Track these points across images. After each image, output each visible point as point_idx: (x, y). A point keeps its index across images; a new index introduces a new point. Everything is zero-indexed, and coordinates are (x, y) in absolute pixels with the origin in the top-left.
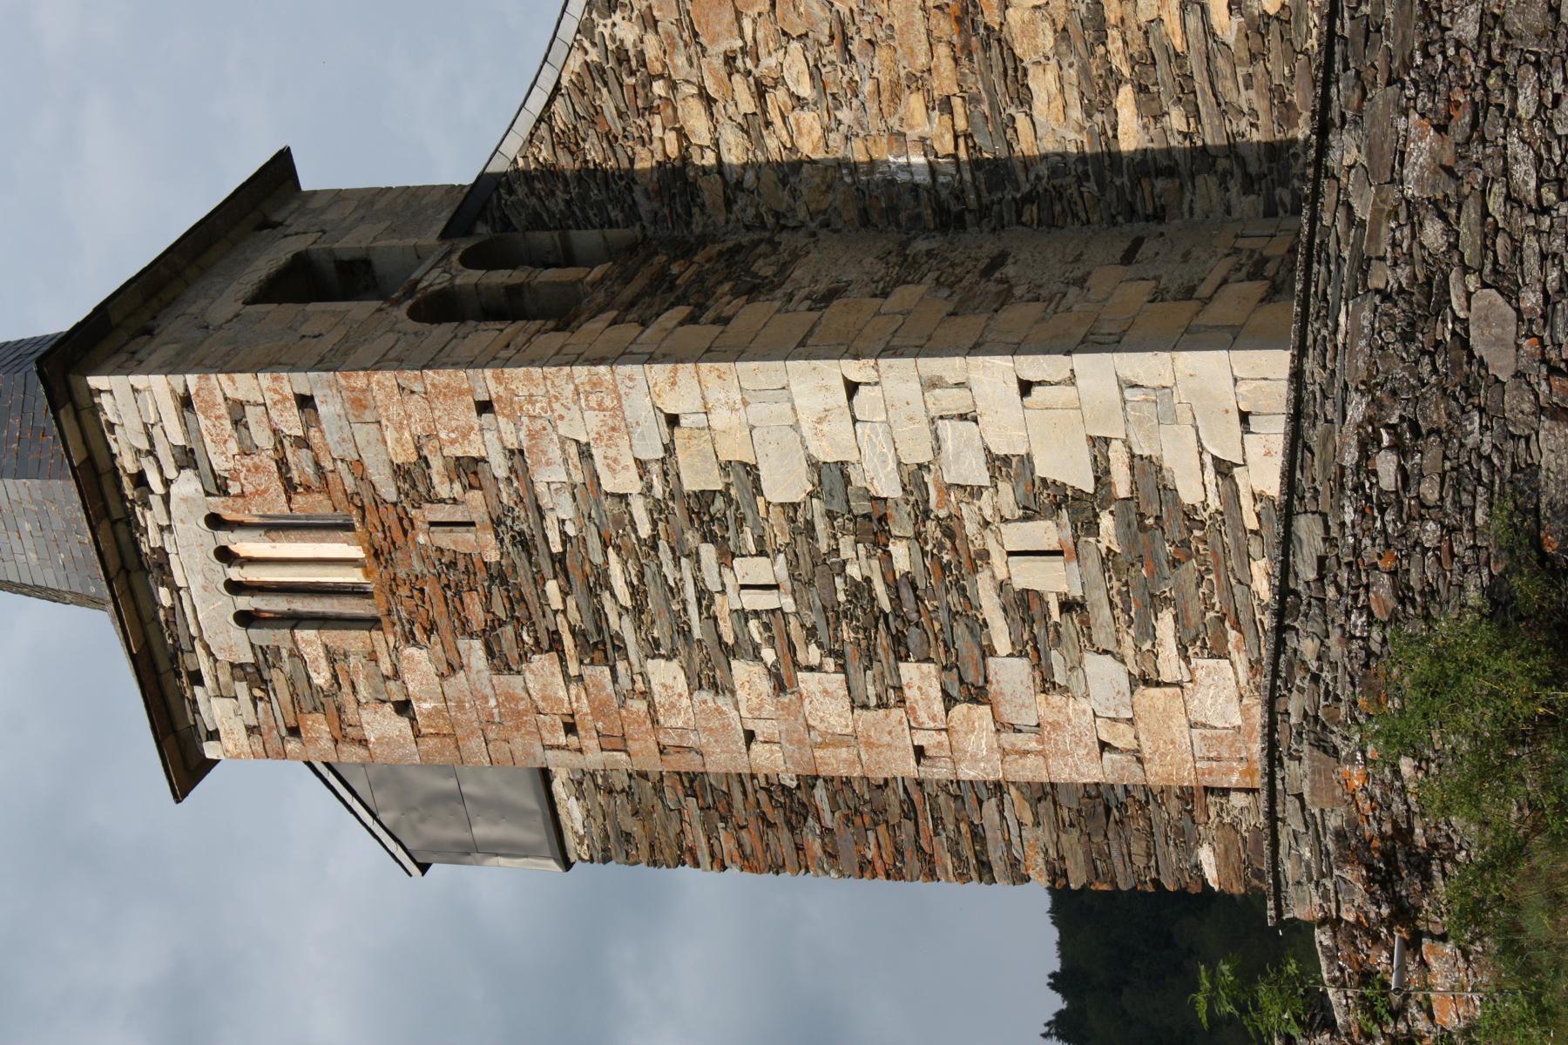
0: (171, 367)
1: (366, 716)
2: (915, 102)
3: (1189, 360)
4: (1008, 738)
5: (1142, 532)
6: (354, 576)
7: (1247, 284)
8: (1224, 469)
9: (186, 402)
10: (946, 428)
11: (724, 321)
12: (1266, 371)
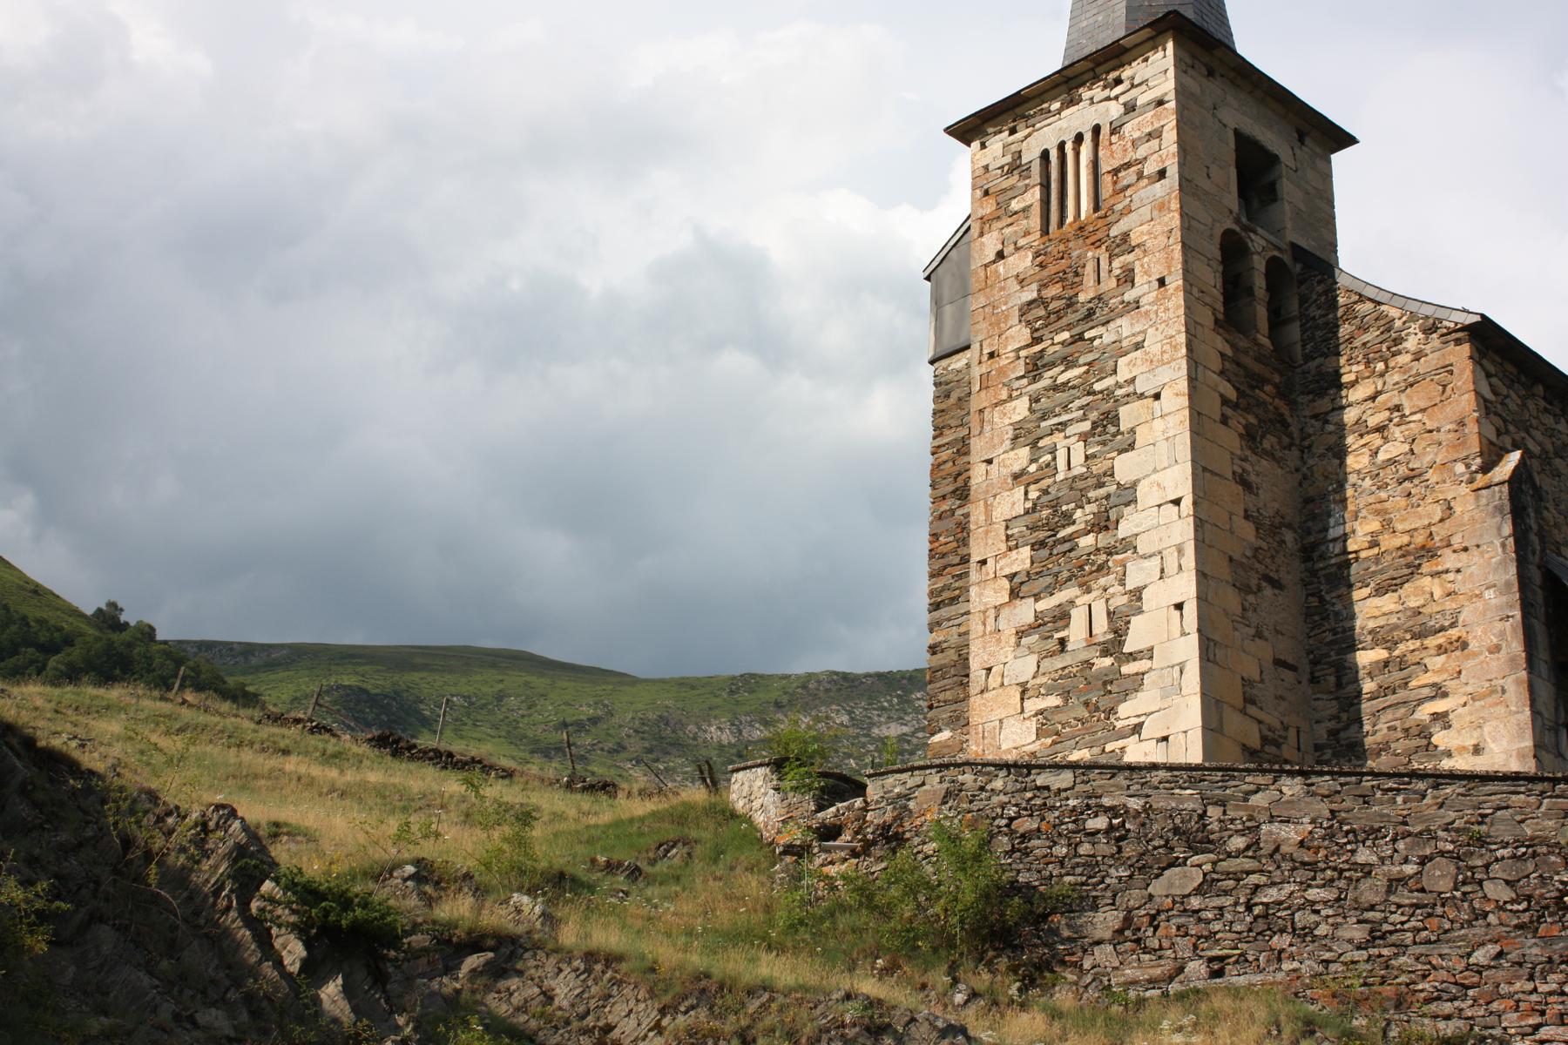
0: (1181, 91)
1: (995, 234)
2: (1375, 525)
3: (1195, 703)
4: (992, 613)
5: (1101, 685)
6: (1070, 219)
7: (1257, 736)
8: (1137, 729)
9: (1160, 103)
10: (1156, 561)
11: (1224, 420)
12: (1191, 751)
